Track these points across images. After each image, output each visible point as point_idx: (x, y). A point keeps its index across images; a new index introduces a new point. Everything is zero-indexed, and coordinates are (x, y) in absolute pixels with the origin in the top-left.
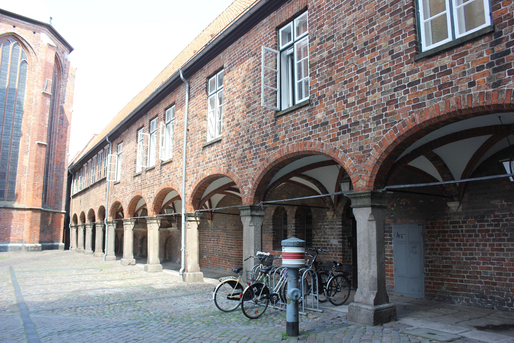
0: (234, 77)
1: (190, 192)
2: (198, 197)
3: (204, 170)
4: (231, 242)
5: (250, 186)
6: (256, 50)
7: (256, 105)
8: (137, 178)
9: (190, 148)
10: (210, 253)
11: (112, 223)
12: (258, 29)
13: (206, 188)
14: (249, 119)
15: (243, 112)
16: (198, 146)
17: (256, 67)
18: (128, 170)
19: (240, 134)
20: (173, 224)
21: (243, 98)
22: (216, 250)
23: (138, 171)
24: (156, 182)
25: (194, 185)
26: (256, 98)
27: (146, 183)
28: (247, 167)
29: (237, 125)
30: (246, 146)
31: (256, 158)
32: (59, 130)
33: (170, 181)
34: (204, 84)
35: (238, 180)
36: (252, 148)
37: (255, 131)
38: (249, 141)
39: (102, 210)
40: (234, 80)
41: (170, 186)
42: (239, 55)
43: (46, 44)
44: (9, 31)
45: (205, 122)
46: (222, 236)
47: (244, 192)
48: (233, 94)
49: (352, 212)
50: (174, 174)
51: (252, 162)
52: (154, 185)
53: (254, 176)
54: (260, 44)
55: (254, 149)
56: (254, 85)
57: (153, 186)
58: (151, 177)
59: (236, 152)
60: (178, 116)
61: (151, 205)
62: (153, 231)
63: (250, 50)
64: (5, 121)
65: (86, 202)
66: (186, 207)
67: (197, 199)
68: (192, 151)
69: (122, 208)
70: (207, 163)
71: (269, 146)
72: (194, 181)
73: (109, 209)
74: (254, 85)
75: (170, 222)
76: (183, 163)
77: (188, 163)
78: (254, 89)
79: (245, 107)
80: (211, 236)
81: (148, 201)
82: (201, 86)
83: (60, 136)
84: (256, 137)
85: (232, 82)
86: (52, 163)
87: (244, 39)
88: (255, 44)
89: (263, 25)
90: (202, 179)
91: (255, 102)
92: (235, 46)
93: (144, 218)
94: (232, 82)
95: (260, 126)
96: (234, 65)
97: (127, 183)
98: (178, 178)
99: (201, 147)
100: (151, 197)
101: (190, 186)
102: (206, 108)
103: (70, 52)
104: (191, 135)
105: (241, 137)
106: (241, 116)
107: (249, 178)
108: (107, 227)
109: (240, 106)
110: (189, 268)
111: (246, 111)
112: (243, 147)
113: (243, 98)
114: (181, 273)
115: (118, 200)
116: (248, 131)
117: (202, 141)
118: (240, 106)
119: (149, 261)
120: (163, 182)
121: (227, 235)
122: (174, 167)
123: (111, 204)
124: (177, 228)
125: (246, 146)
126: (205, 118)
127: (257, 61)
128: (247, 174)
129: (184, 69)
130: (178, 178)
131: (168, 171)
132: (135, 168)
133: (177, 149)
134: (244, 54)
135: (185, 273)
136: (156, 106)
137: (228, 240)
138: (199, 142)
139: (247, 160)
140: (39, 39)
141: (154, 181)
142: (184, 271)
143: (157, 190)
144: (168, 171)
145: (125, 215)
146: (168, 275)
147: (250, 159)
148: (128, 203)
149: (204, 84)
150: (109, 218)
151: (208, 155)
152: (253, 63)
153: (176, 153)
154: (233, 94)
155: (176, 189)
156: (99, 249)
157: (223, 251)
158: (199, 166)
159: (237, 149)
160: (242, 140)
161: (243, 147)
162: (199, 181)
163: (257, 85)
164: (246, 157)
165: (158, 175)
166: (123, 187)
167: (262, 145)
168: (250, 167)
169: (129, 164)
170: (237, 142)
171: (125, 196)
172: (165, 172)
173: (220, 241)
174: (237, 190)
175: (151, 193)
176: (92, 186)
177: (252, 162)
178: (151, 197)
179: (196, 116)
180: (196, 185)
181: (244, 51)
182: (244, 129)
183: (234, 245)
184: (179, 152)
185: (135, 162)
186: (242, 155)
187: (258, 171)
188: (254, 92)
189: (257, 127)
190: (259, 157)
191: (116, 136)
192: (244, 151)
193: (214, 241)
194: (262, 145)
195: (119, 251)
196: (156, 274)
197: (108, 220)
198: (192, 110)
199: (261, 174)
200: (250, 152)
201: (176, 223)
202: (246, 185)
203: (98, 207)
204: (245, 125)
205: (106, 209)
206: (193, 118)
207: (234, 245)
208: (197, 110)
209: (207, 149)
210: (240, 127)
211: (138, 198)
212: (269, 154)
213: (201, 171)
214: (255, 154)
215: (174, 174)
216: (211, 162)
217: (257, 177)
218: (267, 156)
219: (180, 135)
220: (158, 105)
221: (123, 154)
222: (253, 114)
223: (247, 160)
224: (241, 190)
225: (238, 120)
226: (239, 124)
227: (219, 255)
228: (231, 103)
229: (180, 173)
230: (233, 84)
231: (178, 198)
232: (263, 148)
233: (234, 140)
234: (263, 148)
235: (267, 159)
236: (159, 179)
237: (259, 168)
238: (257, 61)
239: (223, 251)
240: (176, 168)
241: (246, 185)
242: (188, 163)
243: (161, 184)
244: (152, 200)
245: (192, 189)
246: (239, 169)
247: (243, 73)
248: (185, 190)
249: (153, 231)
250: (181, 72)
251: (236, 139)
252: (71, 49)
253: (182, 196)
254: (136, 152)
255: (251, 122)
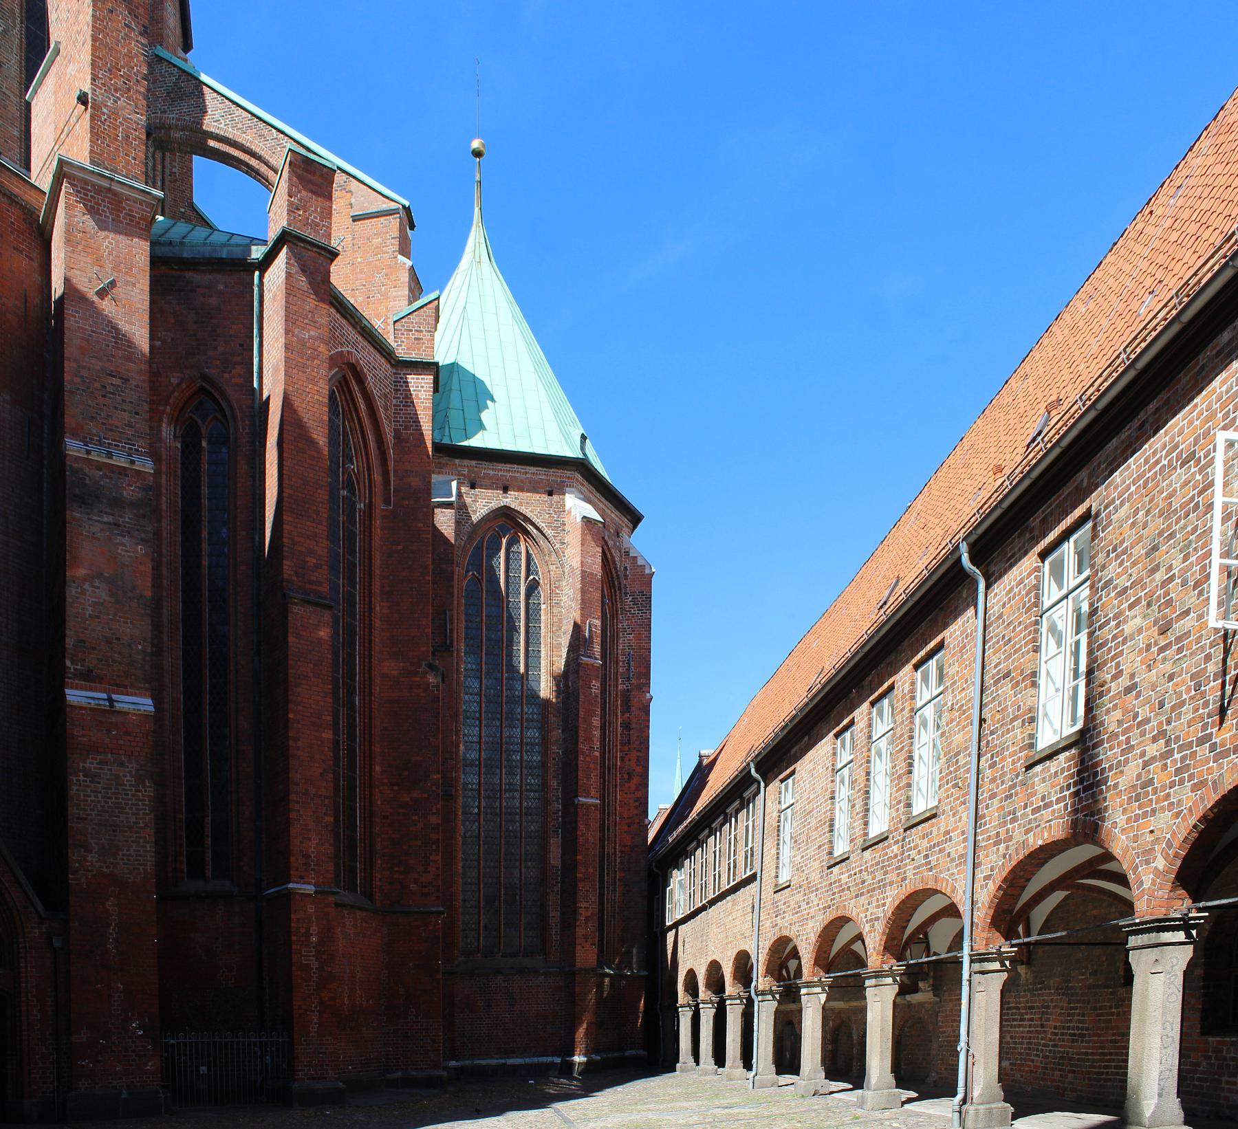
0: (1122, 542)
1: (986, 894)
2: (1006, 907)
3: (1027, 832)
4: (1079, 1021)
5: (1160, 863)
6: (1196, 442)
7: (1188, 622)
8: (836, 870)
9: (988, 773)
10: (1021, 1054)
11: (771, 992)
12: (1202, 368)
13: (1029, 880)
14: (1167, 667)
15: (1148, 647)
16: (1012, 762)
17: (1193, 498)
18: (811, 851)
19: (1136, 715)
20: (921, 984)
21: (1149, 605)
22: (1039, 1044)
23: (840, 849)
24: (892, 876)
25: (999, 876)
26: (1191, 599)
27: (863, 882)
28: (1154, 812)
29: (1128, 690)
30: (1153, 750)
31: (1181, 782)
32: (622, 759)
33: (930, 869)
34: (1029, 575)
35: (1126, 850)
36: (1169, 753)
37: (1183, 703)
38: (1162, 733)
39: (743, 965)
40: (1124, 552)
41: (931, 885)
42: (1139, 467)
43: (579, 519)
44: (494, 505)
45: (1031, 691)
46: (1055, 1007)
47: (1142, 883)
48: (1120, 594)
49: (666, 883)
50: (941, 851)
51: (1168, 795)
52: (884, 886)
53: (1174, 833)
54: (1207, 420)
55: (1177, 756)
56: (1186, 558)
57: (882, 886)
58: (878, 864)
59: (1122, 772)
60: (955, 683)
61: (878, 938)
62: (880, 1005)
63: (1176, 446)
64: (504, 756)
65: (699, 945)
66: (979, 935)
67: (1004, 911)
68: (993, 780)
69: (795, 948)
70: (1036, 810)
71: (1223, 744)
72: (996, 864)
73: (763, 958)
74: (1186, 558)
75: (929, 979)
76: (967, 817)
77: (984, 816)
78: (1184, 571)
79: (1154, 631)
80: (1025, 1008)
81: (867, 928)
82: (1021, 581)
83: (626, 776)
84: (1185, 719)
85: (1117, 557)
86: (611, 851)
87: (1158, 410)
88: (1191, 423)
89: (1219, 353)
90: (1021, 857)
91: (1187, 612)
92: (1129, 437)
93: (859, 975)
94: (1117, 557)
95: (1198, 687)
96: (1122, 504)
97: (810, 888)
98: (953, 860)
99: (1020, 766)
100: (877, 919)
101: (987, 878)
102: (1037, 650)
103: (635, 527)
104: (992, 733)
105: (1140, 725)
106: (1142, 663)
107: (1157, 840)
108: (756, 1004)
109: (1140, 631)
110: (976, 1092)
111: (1156, 644)
112: (1143, 754)
113: (1149, 605)
114: (957, 1108)
115: (786, 933)
116: (1161, 705)
117: (1021, 749)
118: (1140, 631)
119: (869, 1082)
120: (910, 874)
121: (1069, 1002)
122: (943, 829)
123: (766, 944)
124: (931, 994)
125: (1153, 750)
126: (1033, 679)
127: (1198, 477)
128: (1152, 832)
129: (973, 538)
130: (953, 860)
131: (925, 844)
132: (831, 842)
133: (950, 778)
134: (1157, 462)
135: (964, 1107)
136: (888, 660)
137: (1073, 1015)
138: (1015, 753)
139: (1155, 791)
140: (561, 509)
141: (886, 873)
142: (964, 1101)
143: (893, 897)
144: (925, 844)
145: (805, 971)
146: (919, 1115)
147: (1163, 788)
148: (813, 938)
149: (1029, 575)
150: (761, 981)
151: (1041, 788)
152: (1183, 486)
153: (946, 791)
154: (1120, 594)
155: (948, 891)
156: (734, 1061)
157: (1056, 1046)
158: (1014, 820)
159: (1127, 761)
160: (1143, 734)
161: (1143, 754)
162: (1014, 863)
163: (1193, 559)
164: (1150, 782)
165: (896, 856)
166: (799, 897)
167: (1201, 741)
168: (1163, 808)
169: (815, 834)
170: (1128, 740)
171: (803, 921)
172: (916, 847)
173: (1048, 1020)
174: (1122, 879)
175: (878, 907)
176: (713, 902)
177: (1168, 795)
178: (877, 919)
179: (1007, 675)
180: (1004, 874)
181: (1154, 453)
182: (1148, 701)
183: (1087, 1029)
184: (956, 785)
185: (832, 825)
186: (1139, 776)
187: (1184, 819)
188: (1184, 583)
189: (1188, 690)
190: (1191, 777)
191: (778, 757)
192: (1146, 764)
193: (1032, 1020)
194: (1201, 741)
195: (787, 1061)
196: (887, 1114)
197: (761, 988)
198: (995, 660)
199: (1195, 826)
200: (1165, 766)
201: (931, 981)
202: (1147, 862)
203: (732, 954)
204: (1154, 687)
205: (754, 960)
206: (996, 683)
207: (1087, 1029)
208: (1007, 658)
209: (1039, 768)
210: (1138, 695)
211: (841, 922)
212: (1221, 767)
213: (1018, 835)
214: (1178, 771)
215: (941, 851)
216: (1047, 806)
217: (1181, 837)
218: (1215, 775)
219: (958, 738)
220: (893, 656)
221: (797, 807)
222: (1180, 650)
223: (1155, 791)
224: (1131, 877)
225: (1132, 676)
226: (1134, 686)
227: (1046, 1057)
228: (1113, 623)
229: (958, 846)
230: (1121, 564)
231: (951, 911)
232: (1204, 751)
233: (1117, 735)
234: (1204, 751)
235: (1214, 782)
236: (899, 868)
237: (1190, 810)
238: (1198, 477)
239: (1056, 1046)
240: (947, 833)
241: (1147, 862)
242: (984, 816)
243: (904, 879)
244: (880, 927)
245: (992, 887)
246: (1128, 820)
247: (1150, 525)
248: (974, 891)
249: (880, 1005)
250: (964, 548)
251: (1124, 732)
252: (635, 518)
253: (964, 908)
254: (833, 798)
255: (1171, 678)
